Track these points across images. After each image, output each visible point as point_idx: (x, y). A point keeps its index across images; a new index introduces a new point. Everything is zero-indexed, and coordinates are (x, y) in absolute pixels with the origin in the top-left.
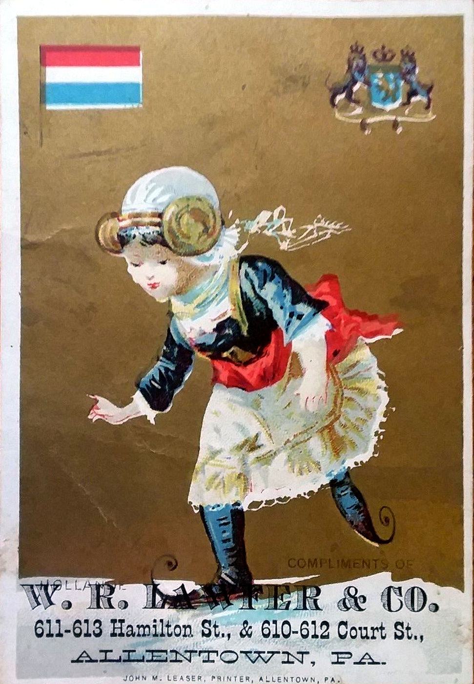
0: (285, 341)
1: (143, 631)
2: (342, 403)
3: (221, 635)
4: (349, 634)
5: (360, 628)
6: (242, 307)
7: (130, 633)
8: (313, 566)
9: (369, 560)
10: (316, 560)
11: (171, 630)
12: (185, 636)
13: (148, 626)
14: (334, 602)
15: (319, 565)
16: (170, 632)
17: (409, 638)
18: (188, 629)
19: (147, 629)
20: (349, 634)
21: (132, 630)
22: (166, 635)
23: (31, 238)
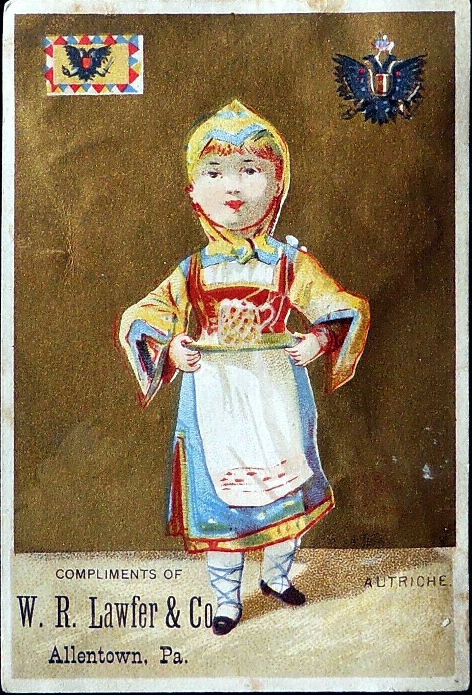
0: (93, 94)
1: (68, 657)
2: (241, 399)
3: (184, 662)
4: (106, 660)
5: (117, 653)
6: (357, 363)
7: (177, 660)
8: (80, 577)
9: (131, 577)
10: (84, 571)
11: (103, 656)
12: (89, 662)
13: (93, 653)
14: (169, 630)
15: (86, 576)
16: (102, 659)
17: (102, 662)
18: (137, 656)
19: (92, 656)
20: (106, 660)
21: (179, 657)
22: (99, 662)
23: (257, 16)
